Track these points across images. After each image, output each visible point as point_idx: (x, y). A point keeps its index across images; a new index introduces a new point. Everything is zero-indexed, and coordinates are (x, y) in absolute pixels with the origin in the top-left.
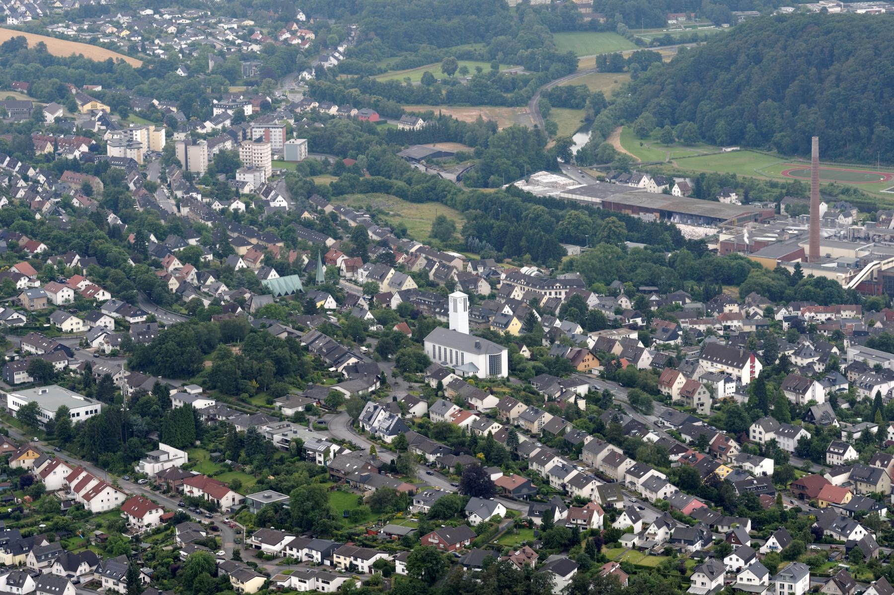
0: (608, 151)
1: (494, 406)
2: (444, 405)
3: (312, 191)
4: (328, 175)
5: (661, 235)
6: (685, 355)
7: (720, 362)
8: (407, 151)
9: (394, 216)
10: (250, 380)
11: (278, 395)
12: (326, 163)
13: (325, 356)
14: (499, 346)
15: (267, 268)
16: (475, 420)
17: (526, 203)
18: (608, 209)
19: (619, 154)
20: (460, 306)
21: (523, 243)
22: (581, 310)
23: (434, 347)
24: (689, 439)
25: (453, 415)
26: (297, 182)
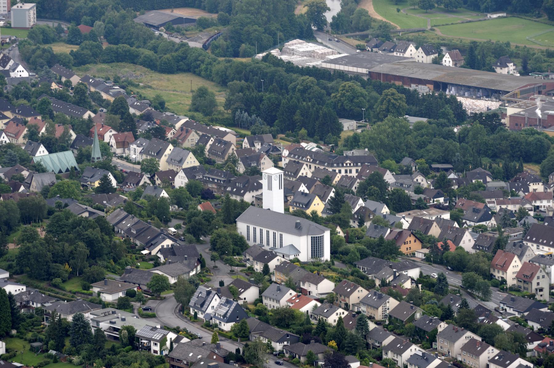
0: (363, 18)
1: (330, 291)
2: (279, 290)
3: (53, 60)
4: (62, 44)
5: (439, 106)
6: (508, 237)
7: (547, 245)
8: (143, 17)
9: (144, 87)
10: (62, 263)
11: (94, 280)
12: (59, 30)
13: (136, 237)
14: (321, 227)
15: (34, 144)
16: (316, 306)
17: (291, 74)
18: (378, 82)
19: (375, 20)
20: (275, 183)
21: (297, 117)
22: (381, 188)
23: (248, 228)
24: (536, 326)
25: (290, 301)
26: (34, 51)
